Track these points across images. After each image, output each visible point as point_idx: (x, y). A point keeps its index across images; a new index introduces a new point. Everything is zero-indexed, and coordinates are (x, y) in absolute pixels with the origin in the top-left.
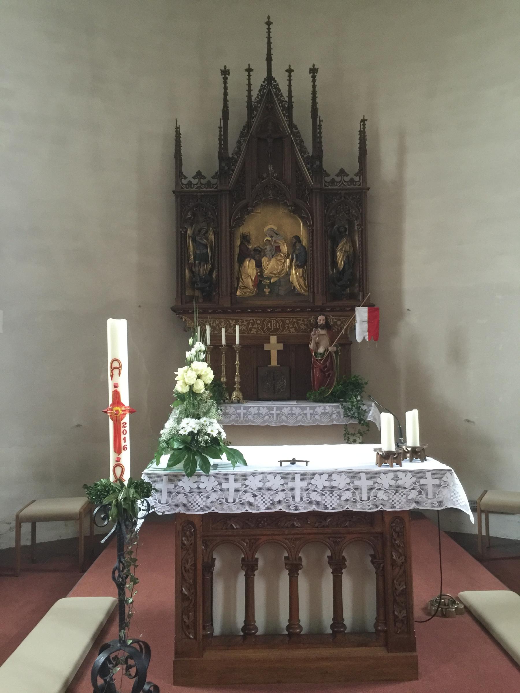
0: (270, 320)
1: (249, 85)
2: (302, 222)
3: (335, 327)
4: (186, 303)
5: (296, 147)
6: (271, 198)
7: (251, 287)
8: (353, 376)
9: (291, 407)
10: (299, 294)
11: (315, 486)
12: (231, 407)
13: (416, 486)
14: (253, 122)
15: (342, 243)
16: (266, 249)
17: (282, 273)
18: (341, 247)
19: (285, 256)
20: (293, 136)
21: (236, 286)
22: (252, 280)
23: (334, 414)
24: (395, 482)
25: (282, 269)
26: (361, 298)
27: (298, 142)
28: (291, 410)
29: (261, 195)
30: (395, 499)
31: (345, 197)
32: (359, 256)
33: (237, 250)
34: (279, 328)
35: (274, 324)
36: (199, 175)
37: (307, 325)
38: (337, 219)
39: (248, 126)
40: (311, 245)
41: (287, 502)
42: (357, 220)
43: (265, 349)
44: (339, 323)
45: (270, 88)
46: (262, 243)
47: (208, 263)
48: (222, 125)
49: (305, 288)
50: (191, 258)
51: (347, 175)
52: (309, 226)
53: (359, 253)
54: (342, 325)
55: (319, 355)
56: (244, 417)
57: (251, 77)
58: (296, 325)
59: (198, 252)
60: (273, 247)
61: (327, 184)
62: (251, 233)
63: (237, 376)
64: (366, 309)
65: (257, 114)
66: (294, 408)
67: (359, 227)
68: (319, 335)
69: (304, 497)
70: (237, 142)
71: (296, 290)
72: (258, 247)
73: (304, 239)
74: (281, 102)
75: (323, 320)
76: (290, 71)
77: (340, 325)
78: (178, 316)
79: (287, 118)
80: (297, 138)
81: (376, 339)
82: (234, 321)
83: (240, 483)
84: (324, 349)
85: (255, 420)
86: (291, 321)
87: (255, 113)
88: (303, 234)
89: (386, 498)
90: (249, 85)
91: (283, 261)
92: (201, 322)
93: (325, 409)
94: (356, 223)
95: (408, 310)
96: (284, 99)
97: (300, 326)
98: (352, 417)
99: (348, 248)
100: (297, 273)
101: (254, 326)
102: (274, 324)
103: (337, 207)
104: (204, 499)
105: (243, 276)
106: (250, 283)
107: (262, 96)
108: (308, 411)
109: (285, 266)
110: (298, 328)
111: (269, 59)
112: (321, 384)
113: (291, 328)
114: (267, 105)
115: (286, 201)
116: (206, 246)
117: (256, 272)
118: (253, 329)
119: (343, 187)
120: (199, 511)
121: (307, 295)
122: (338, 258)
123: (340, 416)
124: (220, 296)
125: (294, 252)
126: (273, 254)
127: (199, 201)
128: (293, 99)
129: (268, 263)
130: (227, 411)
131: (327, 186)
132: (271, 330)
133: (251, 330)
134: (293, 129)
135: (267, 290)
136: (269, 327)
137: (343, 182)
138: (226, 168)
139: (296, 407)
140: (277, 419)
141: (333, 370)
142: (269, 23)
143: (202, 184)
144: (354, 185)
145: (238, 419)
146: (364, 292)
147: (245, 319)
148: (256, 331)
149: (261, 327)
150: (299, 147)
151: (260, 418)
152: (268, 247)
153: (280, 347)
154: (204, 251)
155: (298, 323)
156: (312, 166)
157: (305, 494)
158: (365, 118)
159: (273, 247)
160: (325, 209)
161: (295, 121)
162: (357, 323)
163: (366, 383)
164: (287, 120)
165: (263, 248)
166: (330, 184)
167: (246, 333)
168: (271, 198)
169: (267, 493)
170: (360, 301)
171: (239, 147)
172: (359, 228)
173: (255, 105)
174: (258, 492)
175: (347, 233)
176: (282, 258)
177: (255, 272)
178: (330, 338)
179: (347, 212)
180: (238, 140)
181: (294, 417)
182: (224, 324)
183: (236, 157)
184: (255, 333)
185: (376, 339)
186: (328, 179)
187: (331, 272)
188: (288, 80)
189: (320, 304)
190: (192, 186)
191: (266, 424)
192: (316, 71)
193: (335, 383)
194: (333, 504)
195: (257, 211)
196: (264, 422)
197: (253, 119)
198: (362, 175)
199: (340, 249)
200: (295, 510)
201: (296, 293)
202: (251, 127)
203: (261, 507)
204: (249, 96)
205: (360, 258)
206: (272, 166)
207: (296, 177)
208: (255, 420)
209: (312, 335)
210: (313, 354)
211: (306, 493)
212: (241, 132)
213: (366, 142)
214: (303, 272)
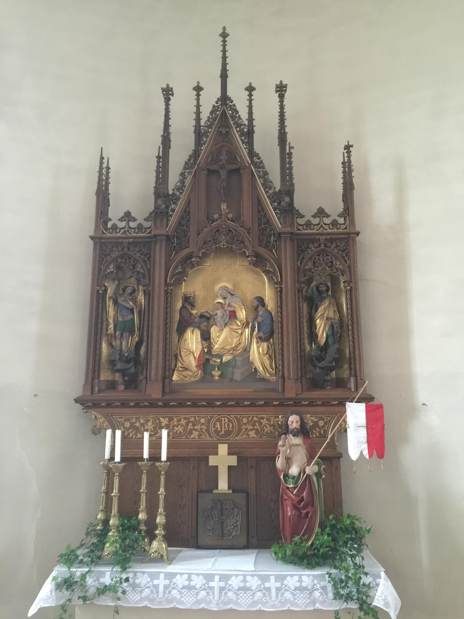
0: (219, 419)
1: (198, 106)
2: (267, 278)
3: (316, 431)
4: (100, 391)
5: (258, 180)
6: (224, 245)
7: (195, 369)
8: (345, 516)
9: (245, 576)
10: (263, 380)
12: (143, 573)
13: (262, 588)
14: (202, 150)
15: (323, 307)
16: (216, 314)
17: (237, 349)
18: (322, 313)
19: (243, 324)
20: (255, 168)
21: (173, 367)
22: (195, 358)
23: (317, 589)
25: (239, 343)
26: (352, 385)
27: (261, 174)
28: (245, 581)
29: (210, 241)
31: (325, 245)
32: (348, 326)
33: (177, 317)
34: (233, 430)
35: (225, 424)
36: (128, 216)
37: (274, 425)
38: (314, 274)
39: (196, 154)
40: (279, 309)
42: (343, 275)
43: (210, 464)
44: (321, 423)
45: (224, 110)
46: (211, 308)
47: (134, 335)
48: (161, 155)
49: (271, 370)
50: (110, 327)
51: (328, 216)
52: (276, 283)
53: (348, 320)
54: (327, 426)
55: (290, 480)
56: (164, 593)
57: (200, 97)
58: (257, 426)
59: (120, 319)
60: (226, 312)
61: (301, 228)
62: (197, 293)
63: (161, 514)
64: (362, 407)
65: (207, 141)
66: (248, 578)
67: (347, 284)
68: (291, 446)
70: (181, 175)
71: (258, 374)
72: (206, 312)
73: (270, 302)
74: (238, 125)
75: (297, 422)
76: (250, 89)
77: (324, 427)
78: (85, 411)
79: (246, 145)
80: (259, 170)
81: (381, 455)
82: (167, 419)
84: (299, 470)
85: (183, 599)
86: (250, 419)
87: (205, 139)
90: (198, 106)
91: (240, 332)
92: (118, 421)
93: (300, 581)
94: (342, 279)
95: (424, 404)
96: (243, 122)
97: (263, 427)
98: (348, 598)
99: (331, 314)
100: (260, 349)
101: (196, 427)
102: (225, 424)
103: (315, 258)
105: (182, 354)
106: (192, 362)
107: (214, 119)
108: (272, 584)
109: (243, 338)
110: (261, 430)
111: (224, 76)
112: (294, 533)
113: (251, 430)
114: (220, 130)
115: (244, 250)
116: (132, 311)
117: (201, 347)
118: (194, 432)
119: (322, 231)
121: (274, 380)
122: (318, 327)
123: (326, 593)
124: (148, 382)
125: (256, 318)
126: (226, 321)
127: (126, 249)
128: (255, 123)
129: (218, 334)
130: (137, 581)
131: (302, 231)
132: (220, 434)
133: (190, 433)
134: (255, 158)
135: (216, 373)
136: (217, 428)
137: (323, 224)
138: (163, 206)
139: (253, 576)
140: (220, 598)
141: (313, 505)
142: (224, 35)
143: (130, 228)
144: (338, 229)
145: (155, 596)
146: (356, 377)
147: (183, 416)
148: (198, 435)
149: (205, 428)
150: (262, 180)
151: (191, 595)
152: (219, 313)
153: (233, 461)
154: (129, 317)
155: (260, 424)
156: (279, 204)
157: (167, 591)
158: (350, 144)
159: (226, 312)
160: (298, 261)
161: (257, 148)
162: (349, 428)
163: (369, 531)
164: (245, 147)
165: (211, 313)
166: (305, 228)
167: (184, 437)
168: (224, 245)
170: (353, 390)
171: (182, 182)
172: (347, 286)
173: (205, 130)
175: (330, 293)
176: (239, 328)
177: (200, 347)
178: (307, 450)
179: (330, 264)
180: (182, 172)
181: (249, 593)
182: (152, 424)
183: (178, 193)
184: (197, 437)
185: (381, 455)
186: (301, 221)
187: (308, 348)
188: (248, 100)
189: (293, 395)
190: (118, 231)
191: (201, 607)
192: (284, 89)
193: (317, 529)
195: (206, 265)
196: (199, 602)
197: (201, 147)
198: (349, 216)
199: (322, 315)
201: (258, 377)
202: (199, 156)
204: (198, 119)
205: (350, 327)
206: (225, 204)
207: (259, 218)
208: (183, 599)
209: (280, 446)
210: (282, 477)
212: (186, 162)
213: (353, 173)
214: (268, 347)
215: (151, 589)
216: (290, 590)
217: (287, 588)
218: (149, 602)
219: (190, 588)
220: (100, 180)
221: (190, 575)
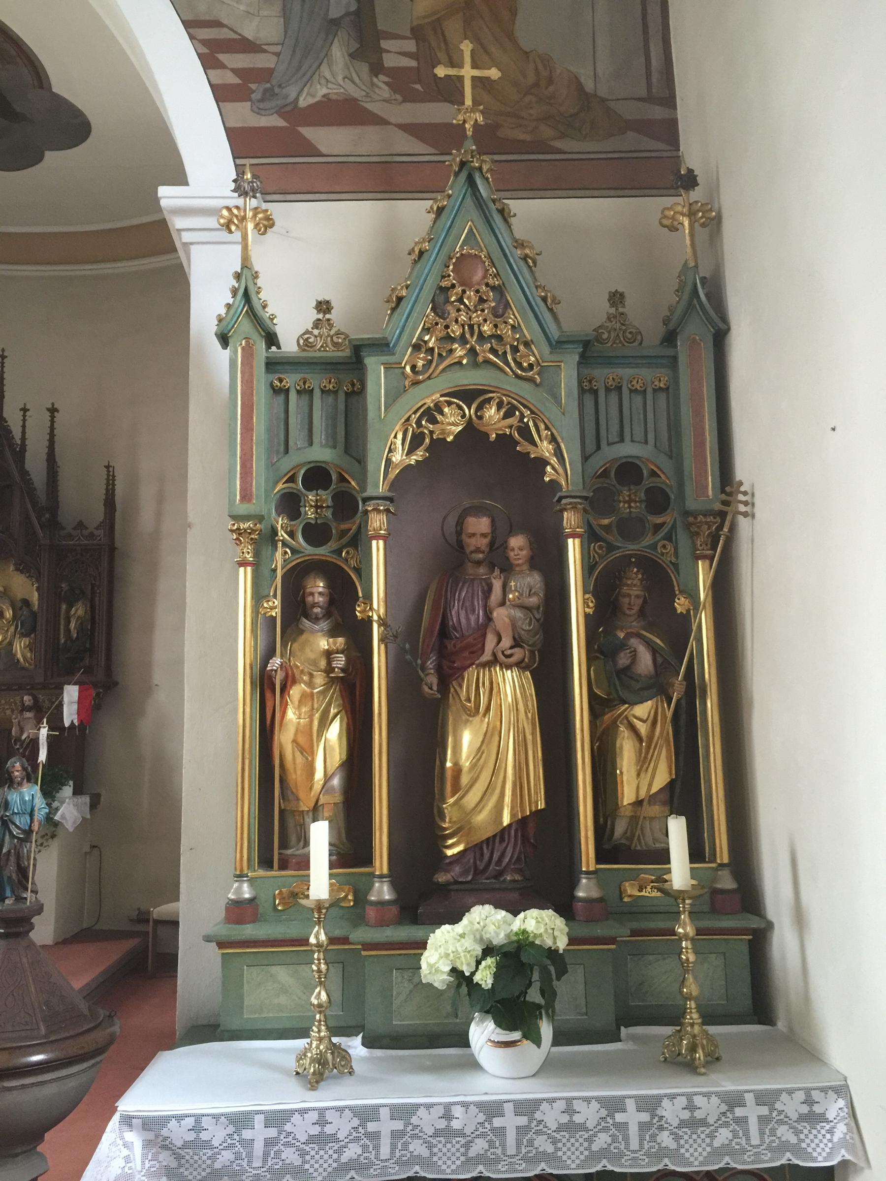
10: (23, 668)
11: (784, 1113)
13: (608, 1125)
24: (195, 1135)
30: (569, 1149)
41: (616, 1151)
51: (86, 528)
64: (76, 688)
69: (147, 1161)
83: (526, 1117)
88: (35, 597)
89: (550, 1149)
104: (335, 1156)
120: (453, 1172)
169: (818, 1127)
174: (438, 1139)
186: (63, 533)
194: (454, 1163)
200: (753, 1162)
203: (444, 1167)
211: (769, 1127)
215: (611, 1132)
216: (670, 1128)
217: (782, 1117)
218: (847, 1151)
219: (571, 1128)
220: (108, 484)
221: (808, 1091)
